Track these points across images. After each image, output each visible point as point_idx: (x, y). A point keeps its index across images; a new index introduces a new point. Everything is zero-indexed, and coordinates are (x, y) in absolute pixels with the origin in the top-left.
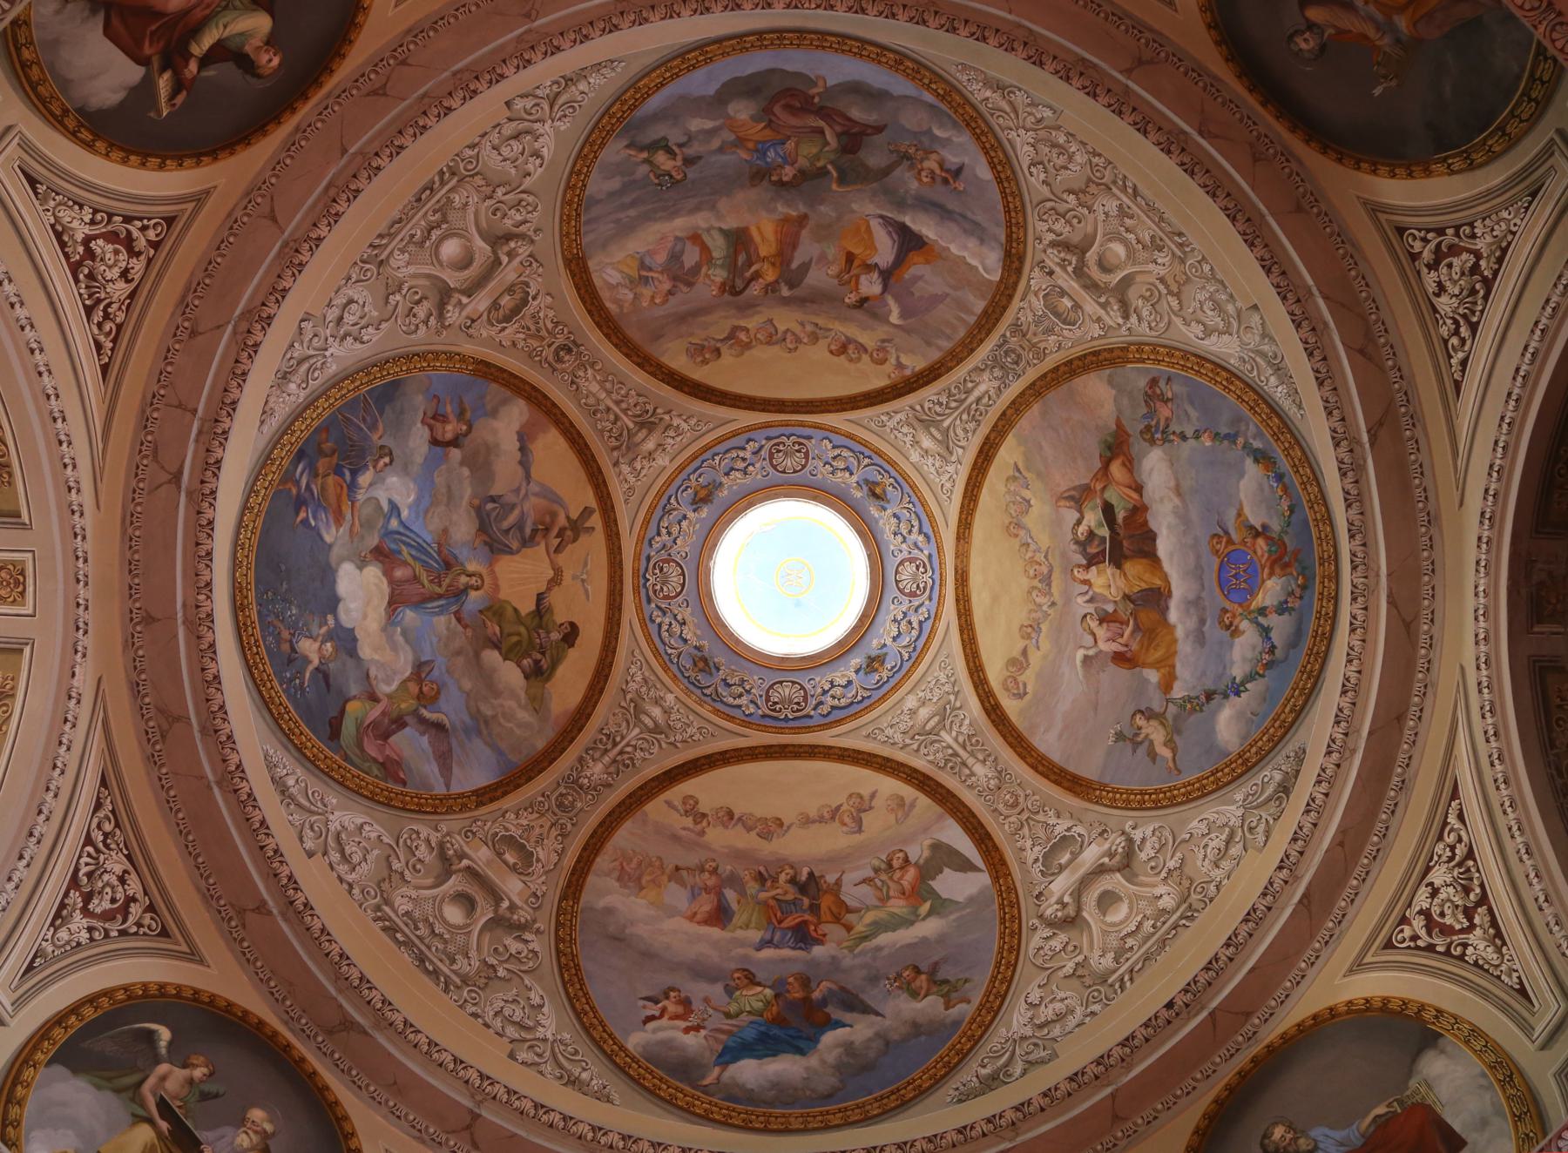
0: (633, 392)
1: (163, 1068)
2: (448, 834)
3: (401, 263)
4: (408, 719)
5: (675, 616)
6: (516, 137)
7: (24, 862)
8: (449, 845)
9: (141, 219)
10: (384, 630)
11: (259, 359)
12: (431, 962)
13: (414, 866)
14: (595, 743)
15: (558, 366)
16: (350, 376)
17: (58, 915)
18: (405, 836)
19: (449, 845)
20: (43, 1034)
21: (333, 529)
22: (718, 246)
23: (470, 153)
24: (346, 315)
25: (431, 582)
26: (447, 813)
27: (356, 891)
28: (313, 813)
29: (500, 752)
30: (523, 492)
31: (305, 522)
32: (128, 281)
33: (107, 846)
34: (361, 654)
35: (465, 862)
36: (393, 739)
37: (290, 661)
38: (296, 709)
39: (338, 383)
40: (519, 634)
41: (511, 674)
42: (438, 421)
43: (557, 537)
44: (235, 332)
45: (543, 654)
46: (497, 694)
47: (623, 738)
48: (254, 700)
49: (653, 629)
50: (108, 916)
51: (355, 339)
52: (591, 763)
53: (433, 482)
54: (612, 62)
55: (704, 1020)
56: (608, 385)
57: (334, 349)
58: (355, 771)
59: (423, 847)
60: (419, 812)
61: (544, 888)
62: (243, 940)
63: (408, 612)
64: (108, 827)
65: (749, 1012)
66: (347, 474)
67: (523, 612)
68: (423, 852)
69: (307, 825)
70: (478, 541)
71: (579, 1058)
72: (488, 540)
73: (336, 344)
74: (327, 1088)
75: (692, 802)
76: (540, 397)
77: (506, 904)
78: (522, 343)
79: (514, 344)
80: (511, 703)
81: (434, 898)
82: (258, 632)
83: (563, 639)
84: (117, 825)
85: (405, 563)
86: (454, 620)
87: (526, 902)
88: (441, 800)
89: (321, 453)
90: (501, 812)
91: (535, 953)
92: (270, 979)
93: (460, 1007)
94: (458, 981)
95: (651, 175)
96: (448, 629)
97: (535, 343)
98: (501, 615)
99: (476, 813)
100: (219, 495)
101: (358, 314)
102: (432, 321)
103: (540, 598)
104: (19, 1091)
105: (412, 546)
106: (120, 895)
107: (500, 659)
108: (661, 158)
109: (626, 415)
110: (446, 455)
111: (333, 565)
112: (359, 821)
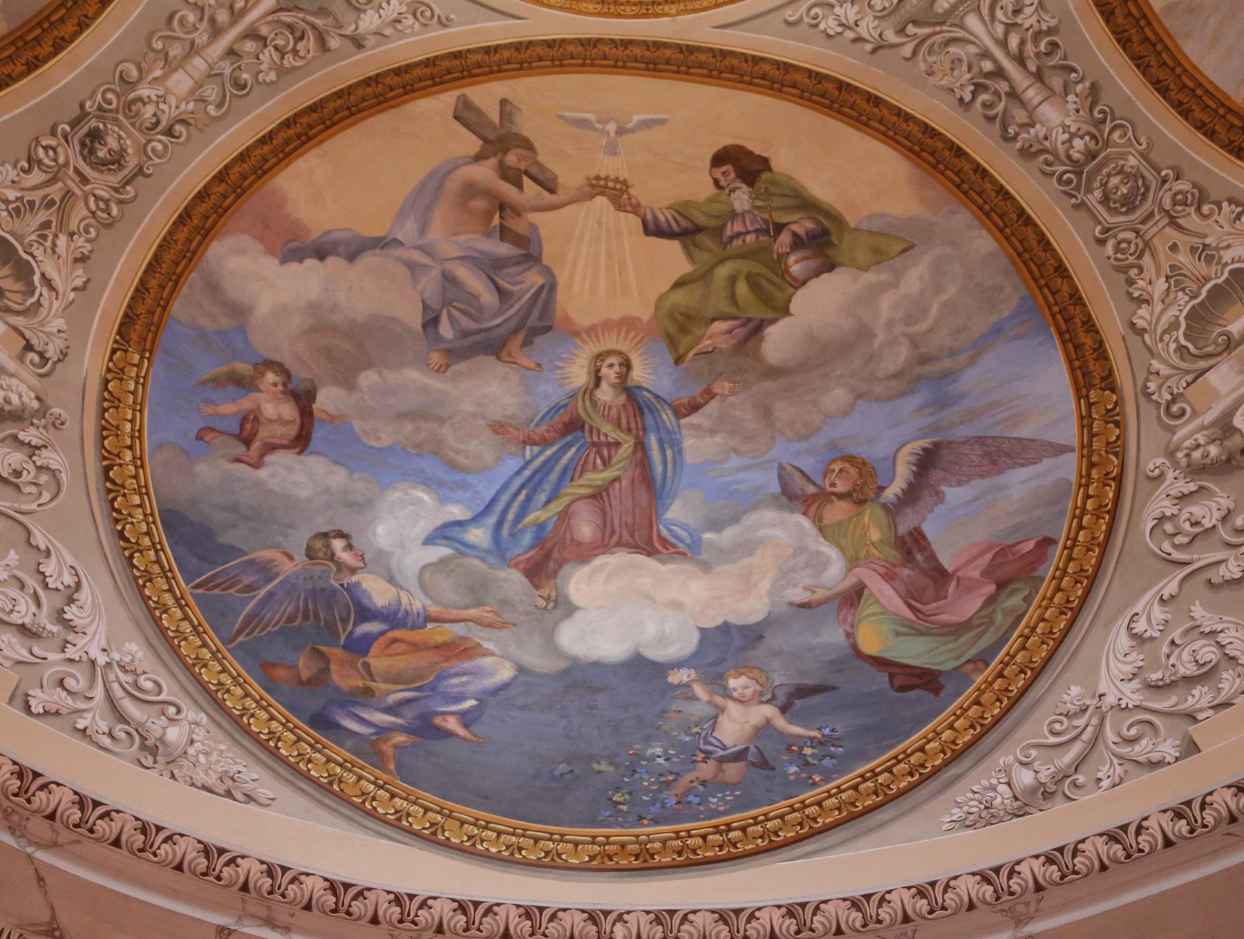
2: (1171, 455)
4: (903, 528)
8: (1197, 455)
10: (706, 567)
11: (111, 798)
14: (991, 119)
15: (131, 163)
16: (154, 613)
18: (1167, 546)
19: (1197, 455)
24: (15, 618)
25: (607, 463)
26: (1121, 456)
29: (996, 331)
30: (417, 256)
31: (467, 719)
36: (948, 563)
37: (763, 763)
38: (864, 757)
40: (733, 280)
42: (253, 434)
43: (520, 186)
44: (53, 846)
45: (779, 228)
46: (864, 333)
47: (986, 55)
48: (843, 843)
51: (71, 600)
52: (1039, 130)
53: (388, 450)
57: (92, 645)
58: (1013, 643)
59: (1197, 510)
60: (1114, 514)
63: (669, 515)
68: (1207, 512)
69: (1124, 750)
70: (525, 361)
72: (520, 338)
73: (81, 642)
76: (203, 208)
78: (80, 241)
79: (82, 259)
80: (886, 304)
83: (751, 184)
85: (565, 516)
86: (694, 419)
88: (1092, 465)
89: (319, 680)
90: (1133, 339)
96: (712, 432)
97: (79, 213)
98: (689, 317)
100: (403, 888)
102: (30, 435)
103: (654, 229)
105: (529, 499)
107: (784, 323)
109: (243, 12)
110: (332, 418)
111: (561, 665)
112: (1124, 642)
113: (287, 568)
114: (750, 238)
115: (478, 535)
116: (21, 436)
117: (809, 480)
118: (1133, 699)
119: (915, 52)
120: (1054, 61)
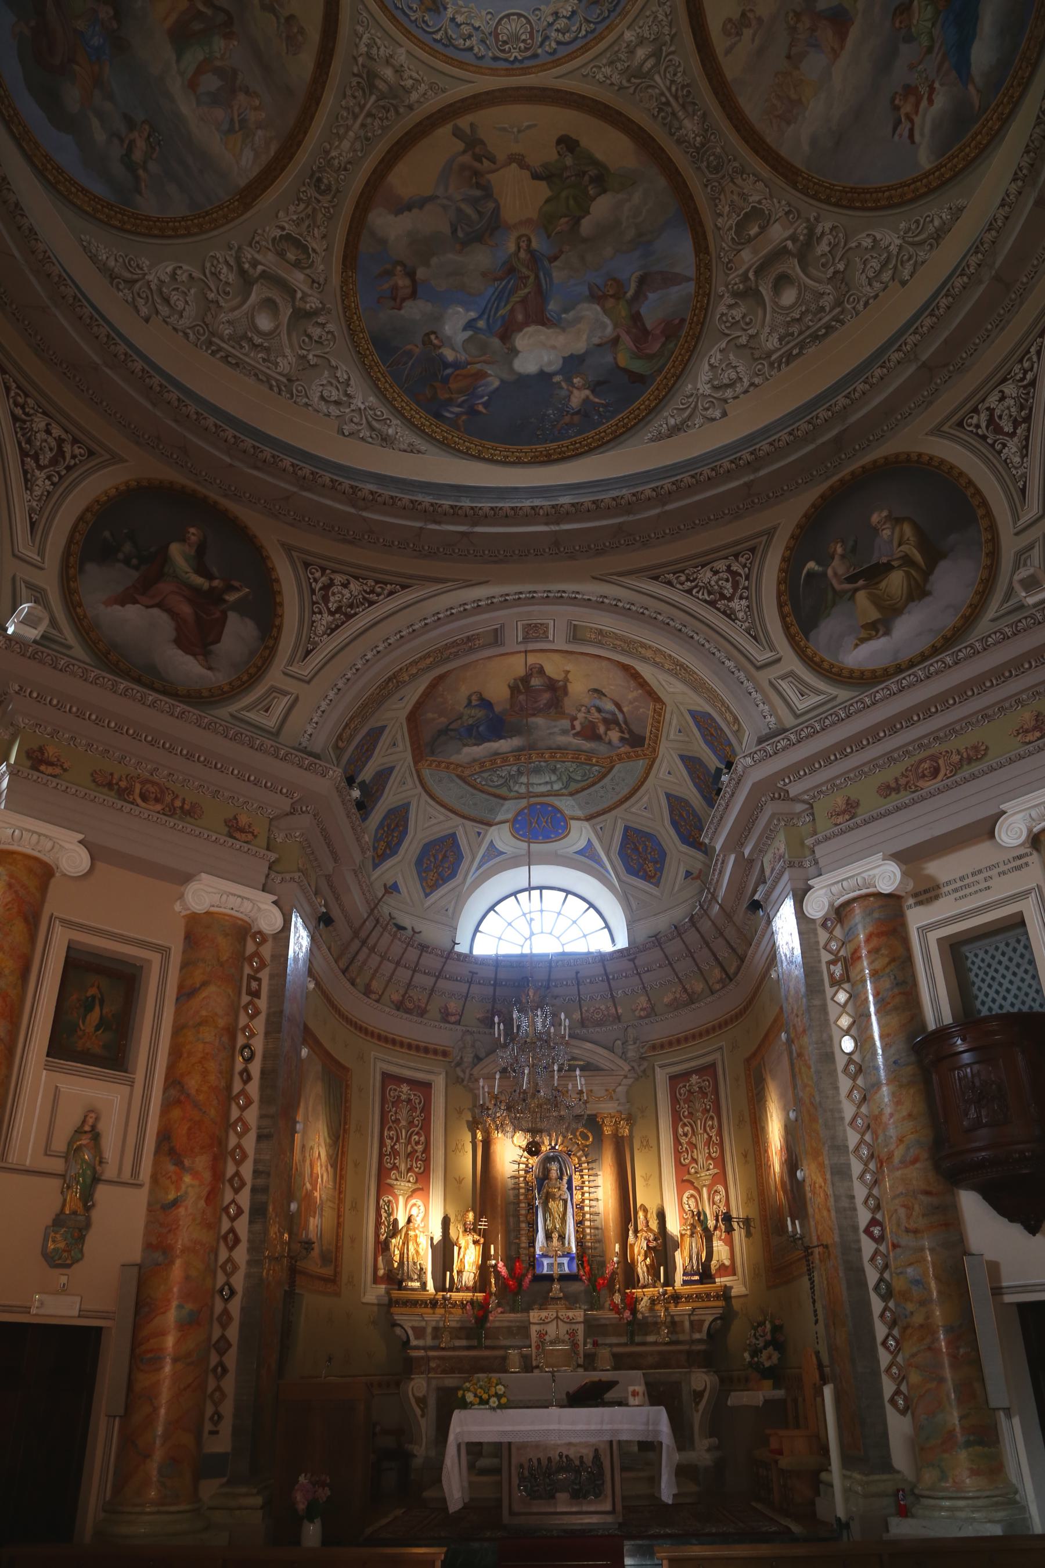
0: (343, 103)
1: (830, 572)
2: (727, 286)
3: (285, 361)
5: (550, 25)
6: (167, 301)
7: (695, 636)
9: (311, 584)
10: (564, 330)
12: (819, 329)
13: (747, 324)
15: (334, 188)
17: (729, 616)
20: (791, 638)
21: (490, 379)
22: (194, 56)
23: (191, 335)
24: (333, 399)
25: (525, 286)
26: (710, 284)
27: (757, 380)
28: (696, 406)
31: (486, 405)
32: (349, 583)
33: (694, 580)
34: (583, 351)
35: (751, 275)
36: (649, 327)
39: (382, 392)
41: (601, 207)
43: (481, 162)
45: (584, 173)
47: (662, 94)
48: (613, 448)
49: (563, 51)
50: (735, 586)
51: (348, 385)
52: (683, 132)
54: (85, 247)
55: (927, 78)
56: (342, 131)
57: (358, 403)
59: (734, 312)
60: (706, 310)
61: (783, 202)
62: (768, 496)
63: (550, 307)
64: (683, 578)
65: (933, 25)
66: (449, 371)
67: (548, 193)
68: (737, 313)
71: (922, 221)
73: (354, 401)
74: (875, 461)
75: (729, 26)
77: (789, 244)
78: (322, 229)
79: (324, 237)
81: (774, 311)
82: (565, 442)
84: (683, 571)
85: (512, 310)
86: (556, 263)
87: (792, 223)
88: (700, 288)
91: (834, 228)
92: (797, 483)
93: (857, 314)
94: (838, 310)
95: (154, 156)
97: (320, 216)
99: (714, 255)
101: (329, 388)
103: (536, 176)
104: (816, 659)
106: (725, 575)
107: (588, 218)
108: (138, 156)
109: (365, 105)
112: (707, 367)
113: (417, 351)
114: (573, 178)
115: (481, 324)
116: (319, 321)
117: (600, 290)
118: (708, 392)
119: (635, 91)
120: (689, 100)
